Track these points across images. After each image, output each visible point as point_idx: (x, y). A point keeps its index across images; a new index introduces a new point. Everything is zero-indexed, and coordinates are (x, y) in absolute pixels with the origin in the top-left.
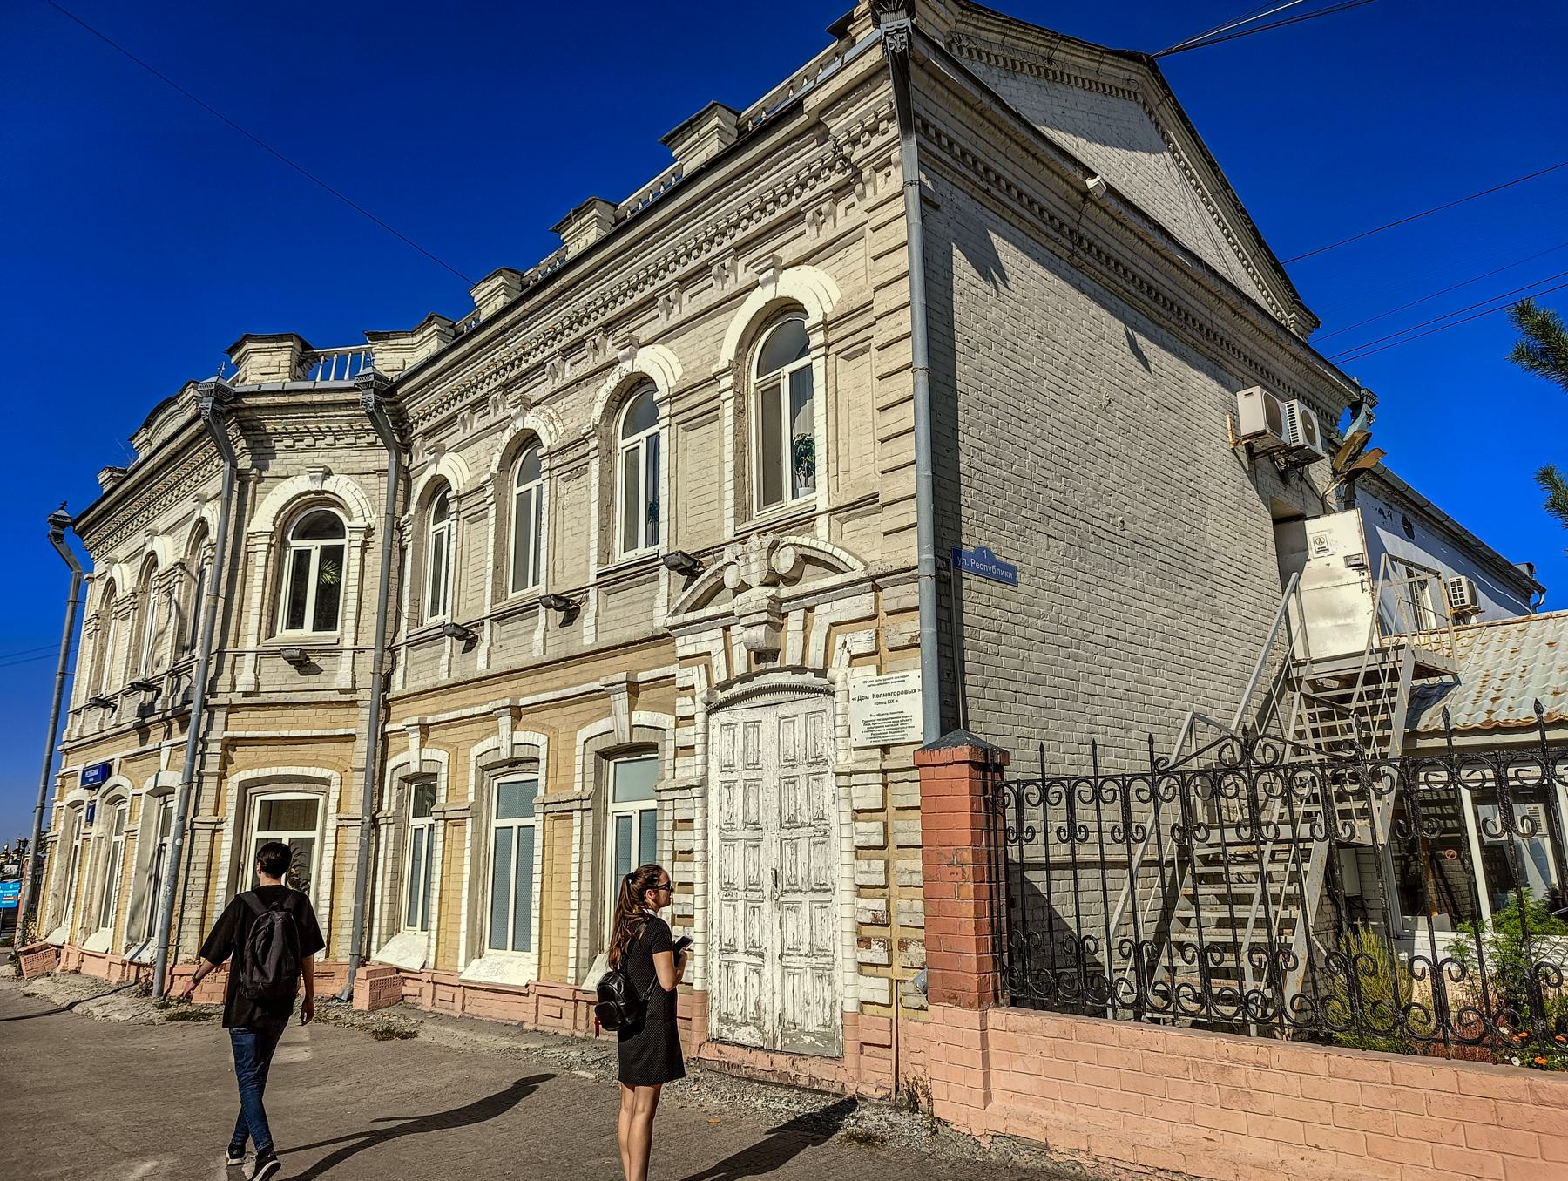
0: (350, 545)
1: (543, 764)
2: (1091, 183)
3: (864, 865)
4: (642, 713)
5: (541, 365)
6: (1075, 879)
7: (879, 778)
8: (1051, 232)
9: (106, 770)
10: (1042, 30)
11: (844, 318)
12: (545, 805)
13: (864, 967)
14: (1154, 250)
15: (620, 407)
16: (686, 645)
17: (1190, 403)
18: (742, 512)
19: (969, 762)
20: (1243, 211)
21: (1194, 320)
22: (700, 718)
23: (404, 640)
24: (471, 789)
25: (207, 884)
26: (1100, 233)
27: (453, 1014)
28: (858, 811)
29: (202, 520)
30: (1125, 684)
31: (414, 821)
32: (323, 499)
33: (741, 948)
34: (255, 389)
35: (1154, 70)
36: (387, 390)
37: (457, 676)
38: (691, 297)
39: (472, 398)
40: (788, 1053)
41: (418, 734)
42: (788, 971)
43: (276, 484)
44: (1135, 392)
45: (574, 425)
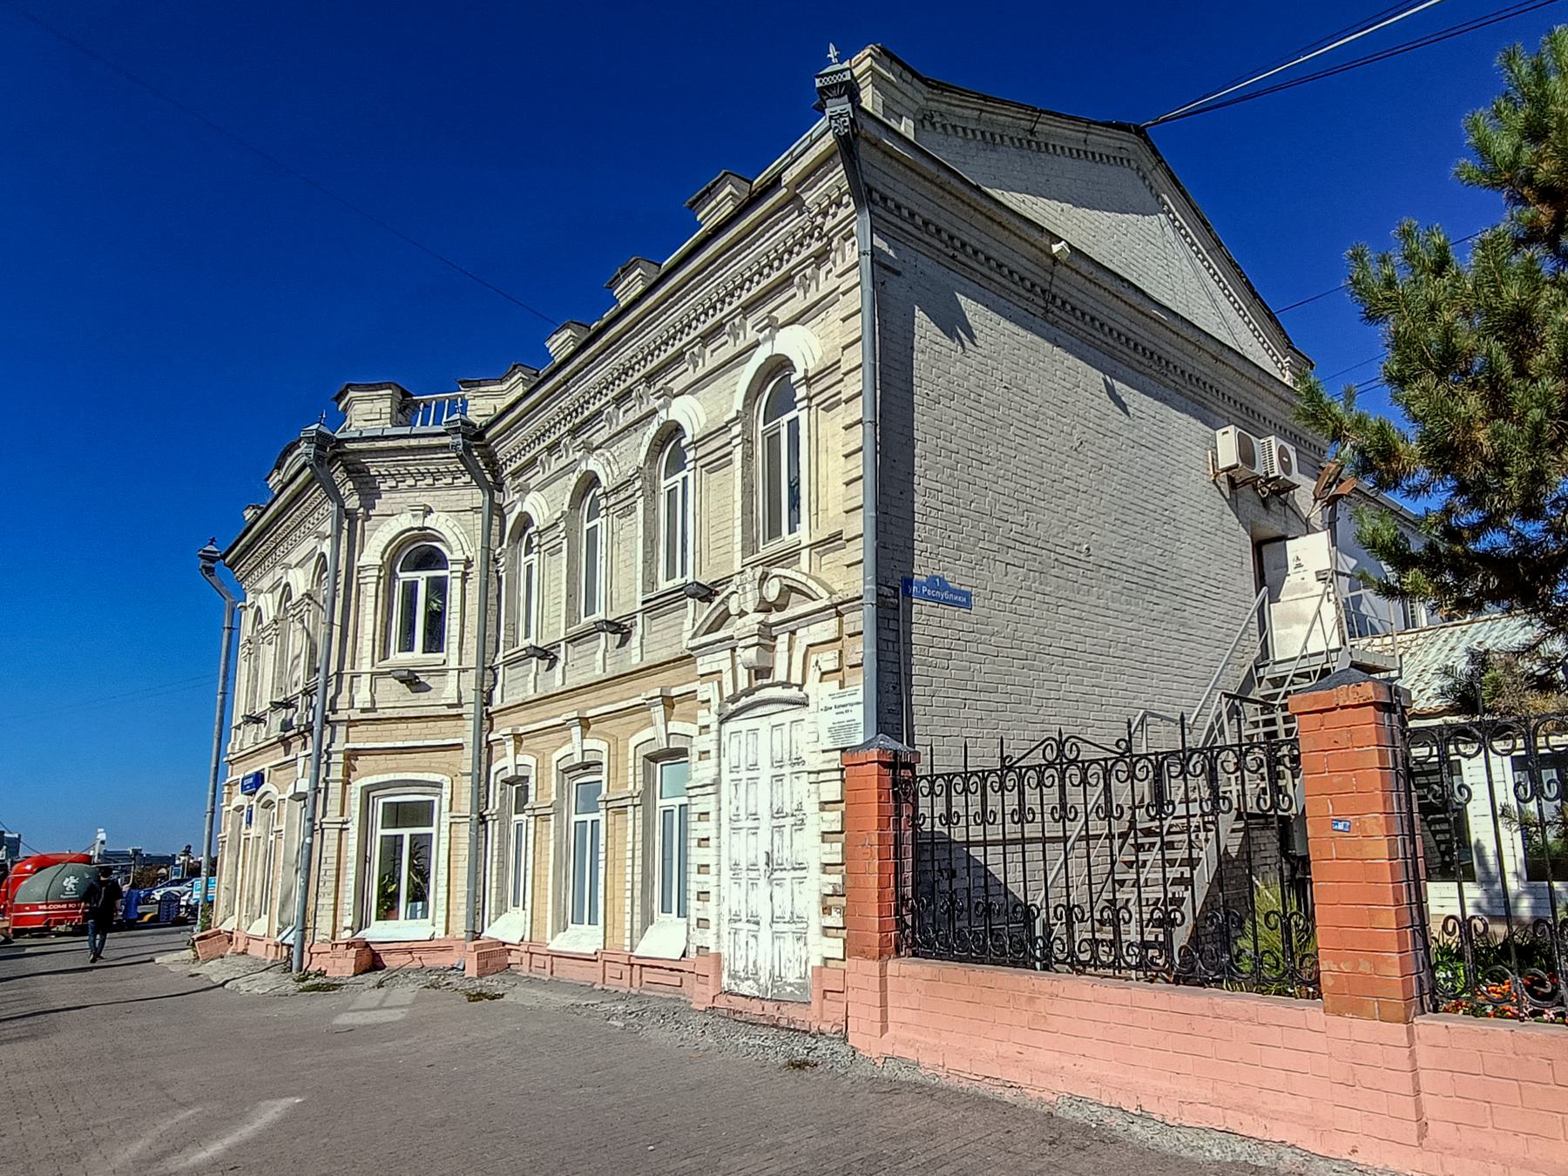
0: (452, 574)
1: (605, 767)
2: (1056, 248)
3: (827, 846)
4: (676, 723)
5: (599, 413)
6: (1024, 852)
7: (837, 775)
8: (1023, 292)
9: (259, 779)
10: (1020, 106)
11: (822, 373)
12: (607, 802)
13: (828, 930)
14: (1130, 306)
15: (662, 450)
16: (704, 664)
17: (1170, 442)
18: (749, 546)
19: (878, 762)
20: (1237, 265)
21: (1175, 367)
22: (714, 726)
23: (501, 660)
24: (554, 789)
25: (338, 876)
26: (1074, 292)
27: (543, 978)
28: (826, 803)
29: (323, 555)
30: (1083, 689)
31: (515, 817)
32: (424, 534)
33: (744, 919)
34: (357, 435)
35: (1147, 140)
36: (474, 436)
37: (541, 692)
38: (713, 351)
39: (548, 441)
40: (776, 1000)
41: (512, 742)
42: (776, 936)
43: (381, 523)
44: (1110, 434)
45: (626, 468)
